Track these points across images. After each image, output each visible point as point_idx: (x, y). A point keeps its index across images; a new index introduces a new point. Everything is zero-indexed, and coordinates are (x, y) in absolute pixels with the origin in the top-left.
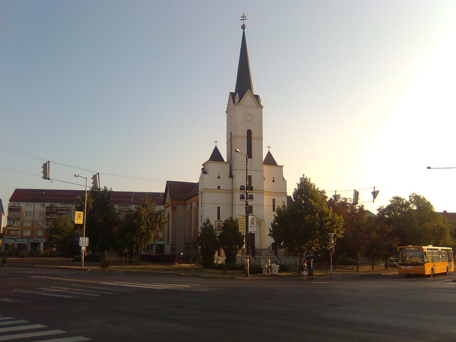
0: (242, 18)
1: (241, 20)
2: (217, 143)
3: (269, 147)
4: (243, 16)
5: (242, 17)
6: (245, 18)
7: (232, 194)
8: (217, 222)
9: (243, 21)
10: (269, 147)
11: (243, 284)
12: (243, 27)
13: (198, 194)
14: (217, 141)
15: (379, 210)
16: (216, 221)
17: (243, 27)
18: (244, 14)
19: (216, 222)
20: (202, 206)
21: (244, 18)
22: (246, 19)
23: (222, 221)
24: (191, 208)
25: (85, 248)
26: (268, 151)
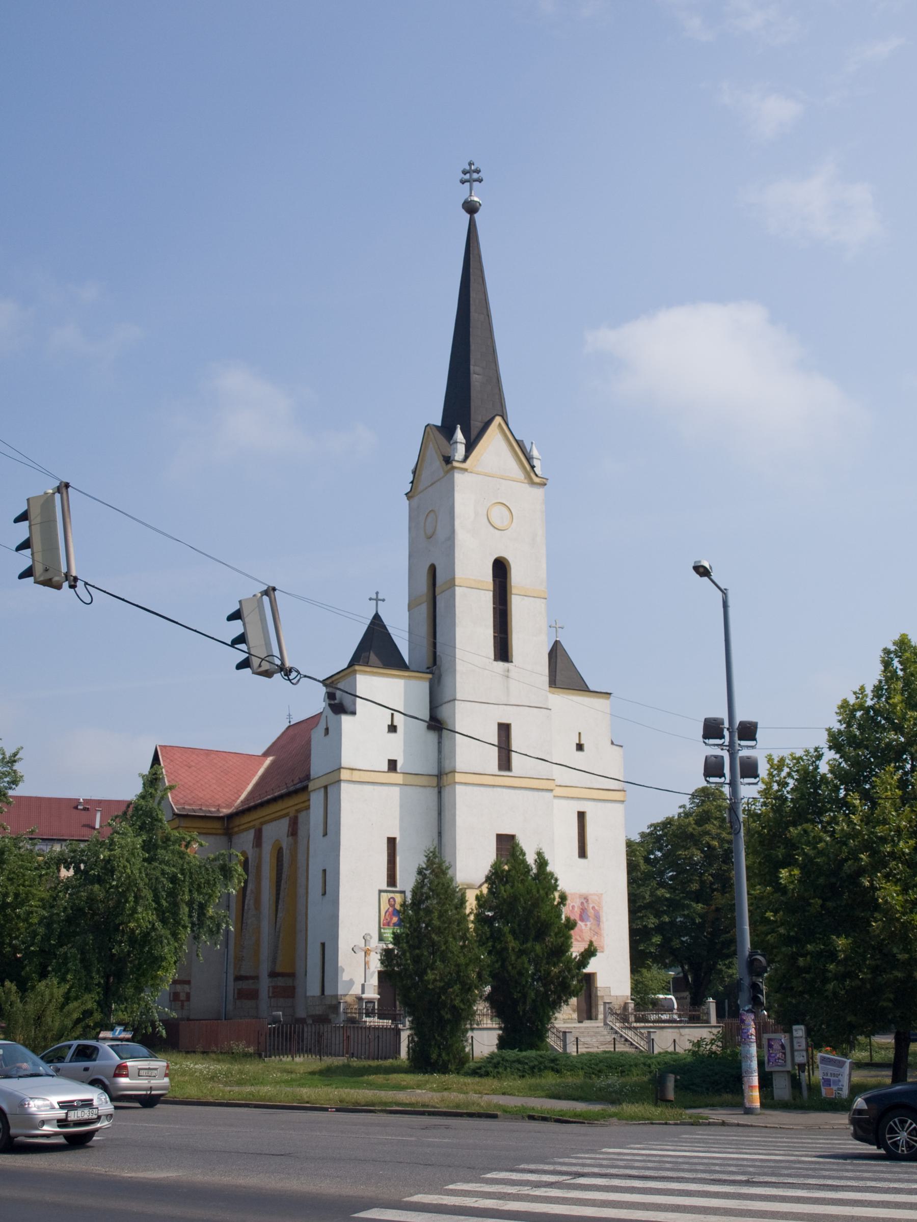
0: (467, 176)
1: (463, 182)
2: (379, 602)
3: (377, 600)
4: (468, 168)
5: (465, 172)
6: (475, 176)
7: (440, 792)
8: (385, 894)
9: (467, 184)
10: (377, 600)
11: (333, 1136)
12: (471, 208)
13: (305, 789)
14: (380, 597)
15: (135, 796)
16: (380, 891)
17: (471, 208)
18: (470, 164)
19: (382, 894)
20: (325, 834)
21: (471, 176)
22: (480, 181)
23: (403, 892)
24: (258, 841)
25: (185, 996)
26: (375, 612)
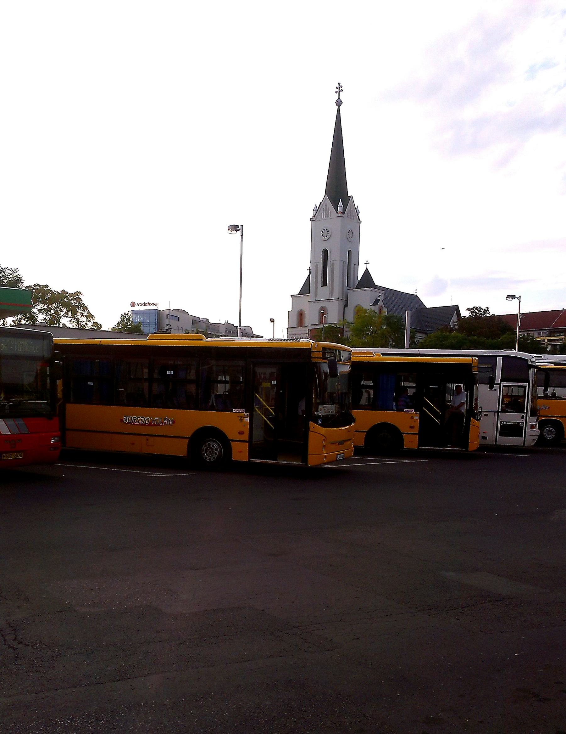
18: (339, 84)
